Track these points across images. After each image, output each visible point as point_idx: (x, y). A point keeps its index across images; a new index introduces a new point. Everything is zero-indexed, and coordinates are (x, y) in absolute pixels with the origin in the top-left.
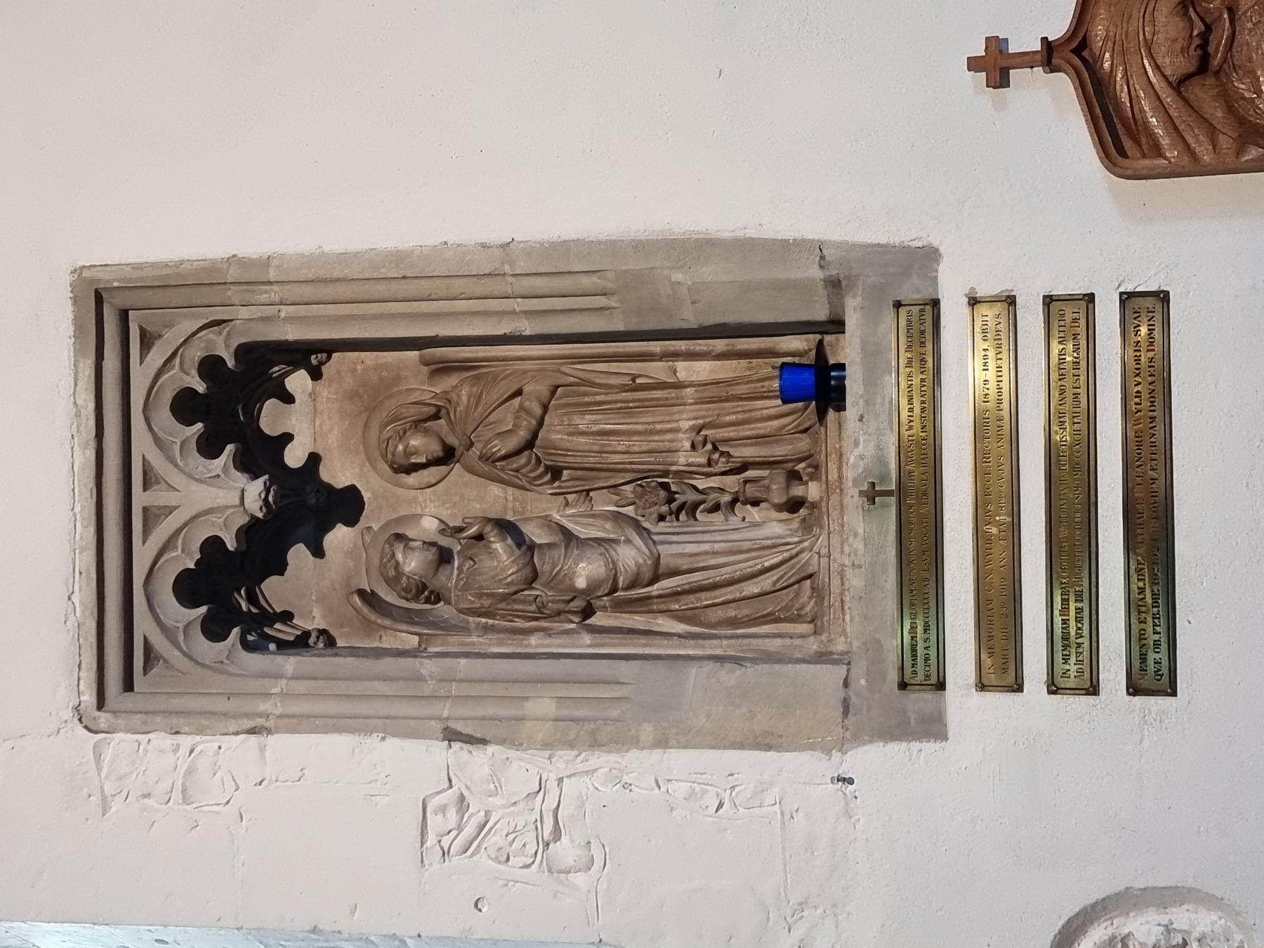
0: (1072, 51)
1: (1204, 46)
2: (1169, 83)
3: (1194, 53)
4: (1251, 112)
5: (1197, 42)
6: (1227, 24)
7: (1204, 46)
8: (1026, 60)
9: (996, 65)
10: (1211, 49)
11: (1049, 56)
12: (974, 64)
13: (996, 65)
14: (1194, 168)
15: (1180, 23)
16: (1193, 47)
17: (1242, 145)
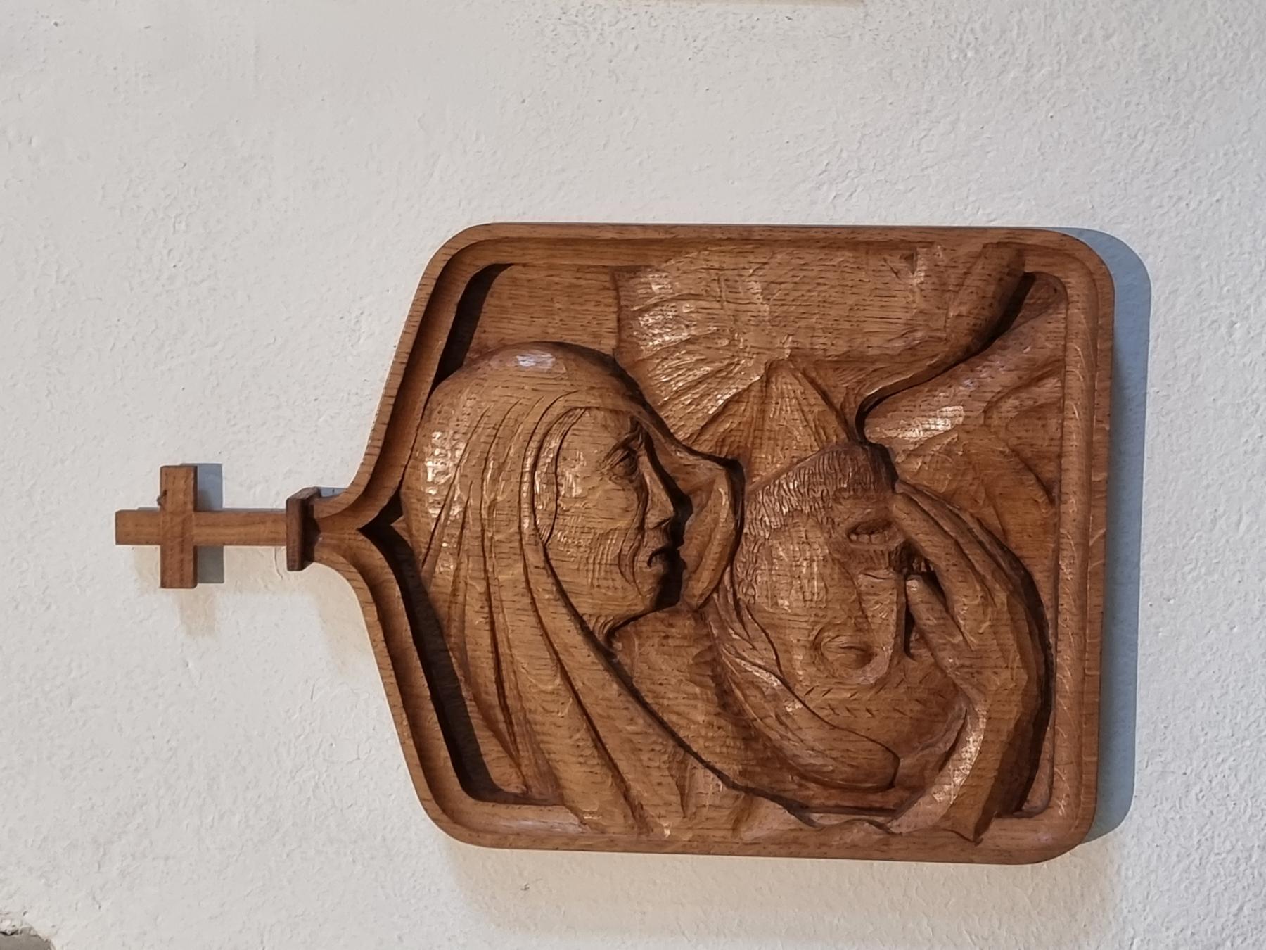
0: (366, 531)
1: (670, 555)
2: (588, 634)
3: (648, 572)
4: (771, 721)
5: (654, 542)
6: (725, 501)
7: (670, 555)
8: (252, 526)
9: (185, 530)
10: (688, 552)
11: (306, 529)
12: (130, 527)
13: (185, 530)
14: (640, 834)
15: (622, 499)
16: (643, 557)
17: (749, 792)
